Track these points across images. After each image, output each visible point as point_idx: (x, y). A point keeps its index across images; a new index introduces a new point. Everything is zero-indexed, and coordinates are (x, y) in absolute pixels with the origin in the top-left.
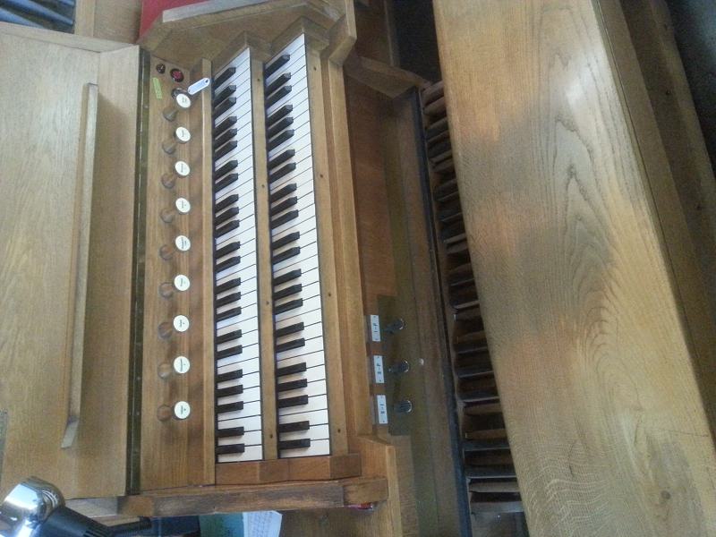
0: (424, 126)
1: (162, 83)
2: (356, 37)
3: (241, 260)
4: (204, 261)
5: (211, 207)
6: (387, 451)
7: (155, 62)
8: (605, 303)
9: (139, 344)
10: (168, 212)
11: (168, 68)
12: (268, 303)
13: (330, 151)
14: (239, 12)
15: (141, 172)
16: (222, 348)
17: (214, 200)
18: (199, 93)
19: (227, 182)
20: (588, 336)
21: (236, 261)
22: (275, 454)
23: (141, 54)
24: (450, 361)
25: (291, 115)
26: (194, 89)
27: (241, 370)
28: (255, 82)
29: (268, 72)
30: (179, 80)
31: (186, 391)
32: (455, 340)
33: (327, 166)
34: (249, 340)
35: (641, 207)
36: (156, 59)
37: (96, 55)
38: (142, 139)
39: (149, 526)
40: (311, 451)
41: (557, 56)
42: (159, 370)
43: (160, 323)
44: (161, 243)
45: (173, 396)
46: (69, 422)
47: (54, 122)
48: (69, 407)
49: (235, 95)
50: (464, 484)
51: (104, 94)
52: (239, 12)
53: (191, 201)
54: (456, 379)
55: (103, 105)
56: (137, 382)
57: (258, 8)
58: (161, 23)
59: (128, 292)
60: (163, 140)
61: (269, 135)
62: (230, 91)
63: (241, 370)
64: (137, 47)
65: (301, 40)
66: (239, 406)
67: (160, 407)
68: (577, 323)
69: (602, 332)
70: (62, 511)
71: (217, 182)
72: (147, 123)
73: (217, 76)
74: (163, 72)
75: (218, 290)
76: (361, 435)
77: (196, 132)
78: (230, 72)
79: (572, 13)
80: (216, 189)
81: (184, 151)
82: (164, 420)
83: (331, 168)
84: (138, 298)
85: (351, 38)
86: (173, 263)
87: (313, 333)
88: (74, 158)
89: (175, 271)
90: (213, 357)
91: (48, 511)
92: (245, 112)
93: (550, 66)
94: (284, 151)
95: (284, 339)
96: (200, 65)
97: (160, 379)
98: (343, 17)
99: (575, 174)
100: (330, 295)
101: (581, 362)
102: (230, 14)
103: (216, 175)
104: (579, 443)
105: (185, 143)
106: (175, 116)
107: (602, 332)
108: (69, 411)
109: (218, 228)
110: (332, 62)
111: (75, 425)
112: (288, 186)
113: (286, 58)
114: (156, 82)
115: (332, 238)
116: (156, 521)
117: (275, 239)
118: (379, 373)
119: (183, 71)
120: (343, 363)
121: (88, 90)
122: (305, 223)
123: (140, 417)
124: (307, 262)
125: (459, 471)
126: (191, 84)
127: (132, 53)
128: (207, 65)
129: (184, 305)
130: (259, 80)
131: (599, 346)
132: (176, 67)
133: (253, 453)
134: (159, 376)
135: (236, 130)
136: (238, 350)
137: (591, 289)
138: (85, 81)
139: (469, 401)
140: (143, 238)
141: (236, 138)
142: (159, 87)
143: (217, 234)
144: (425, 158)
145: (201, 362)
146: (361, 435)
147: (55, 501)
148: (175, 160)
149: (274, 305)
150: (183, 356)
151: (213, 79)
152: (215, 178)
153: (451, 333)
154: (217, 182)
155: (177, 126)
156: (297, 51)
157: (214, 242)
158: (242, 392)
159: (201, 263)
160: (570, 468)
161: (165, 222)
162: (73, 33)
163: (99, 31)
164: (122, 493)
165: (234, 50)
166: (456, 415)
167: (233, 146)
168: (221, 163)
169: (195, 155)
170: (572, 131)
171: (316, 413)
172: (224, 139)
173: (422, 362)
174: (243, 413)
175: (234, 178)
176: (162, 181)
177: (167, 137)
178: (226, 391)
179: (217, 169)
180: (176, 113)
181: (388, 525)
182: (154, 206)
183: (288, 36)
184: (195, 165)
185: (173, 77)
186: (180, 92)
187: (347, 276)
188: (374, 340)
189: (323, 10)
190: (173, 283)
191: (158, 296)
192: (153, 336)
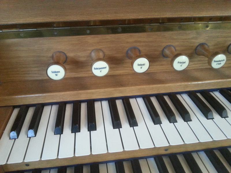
3: (158, 126)
9: (120, 30)
16: (119, 104)
17: (180, 93)
27: (137, 126)
42: (98, 50)
43: (141, 49)
56: (117, 28)
63: (137, 126)
71: (199, 95)
81: (200, 62)
89: (152, 59)
97: (89, 52)
103: (206, 93)
117: (195, 156)
129: (158, 68)
149: (165, 155)
150: (109, 71)
154: (199, 95)
158: (185, 121)
168: (186, 101)
169: (197, 74)
179: (211, 93)
191: (164, 45)
192: (128, 42)
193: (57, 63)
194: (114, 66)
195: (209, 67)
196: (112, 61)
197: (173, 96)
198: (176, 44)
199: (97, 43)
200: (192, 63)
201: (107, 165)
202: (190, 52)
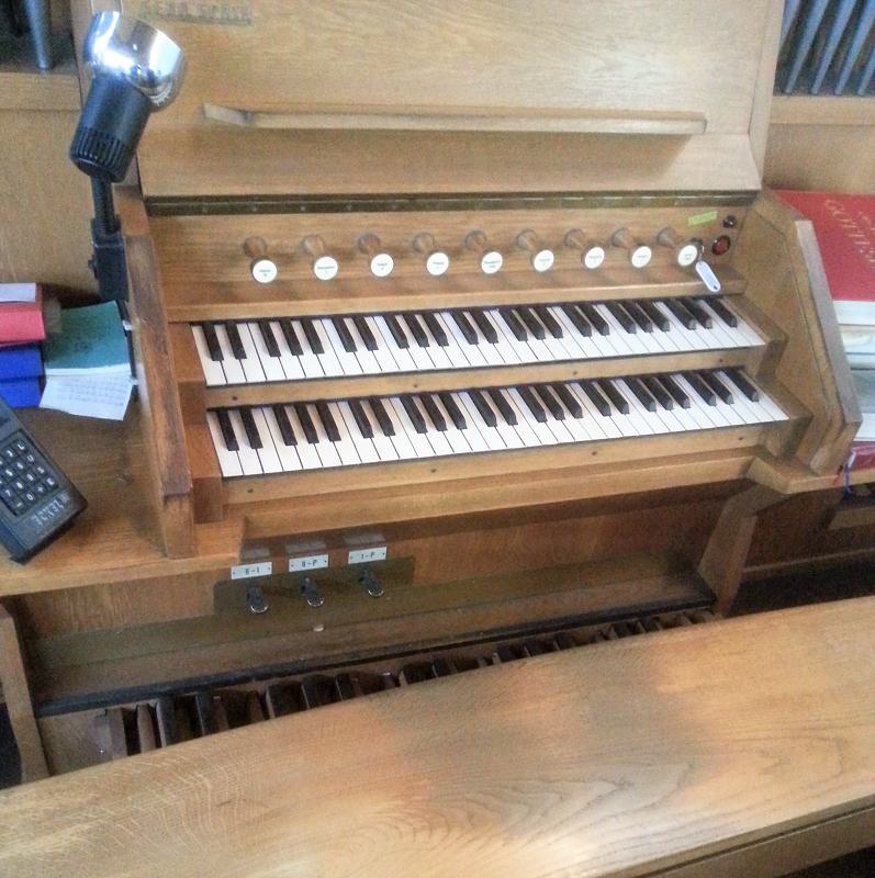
0: (661, 615)
1: (709, 226)
2: (790, 492)
4: (468, 295)
5: (543, 301)
6: (231, 555)
7: (739, 213)
8: (456, 833)
10: (532, 240)
13: (629, 464)
14: (814, 328)
15: (590, 199)
18: (699, 278)
20: (410, 814)
21: (472, 339)
22: (213, 405)
23: (747, 192)
24: (325, 668)
25: (677, 407)
26: (704, 270)
28: (717, 356)
29: (734, 373)
30: (717, 250)
31: (285, 277)
32: (357, 674)
33: (610, 460)
34: (364, 361)
35: (586, 870)
37: (746, 129)
38: (632, 199)
39: (108, 231)
40: (223, 453)
41: (768, 763)
43: (381, 237)
45: (283, 259)
46: (244, 113)
47: (650, 73)
48: (268, 113)
49: (699, 328)
50: (150, 696)
51: (692, 140)
52: (814, 328)
53: (547, 273)
54: (298, 678)
55: (674, 142)
57: (821, 353)
59: (420, 188)
60: (630, 228)
61: (646, 378)
64: (759, 187)
65: (779, 415)
66: (273, 351)
67: (263, 241)
68: (424, 800)
69: (415, 831)
70: (147, 108)
72: (652, 205)
74: (726, 225)
75: (306, 322)
76: (247, 521)
77: (644, 275)
78: (729, 319)
79: (836, 777)
82: (246, 246)
84: (411, 203)
85: (787, 485)
87: (380, 448)
88: (600, 104)
89: (454, 254)
90: (387, 310)
92: (677, 341)
93: (764, 753)
95: (371, 413)
97: (301, 239)
99: (621, 789)
100: (434, 471)
101: (372, 810)
102: (811, 316)
104: (263, 810)
105: (583, 261)
106: (664, 245)
107: (415, 831)
108: (260, 112)
109: (514, 312)
111: (238, 120)
113: (754, 396)
114: (711, 215)
115: (510, 471)
116: (116, 241)
118: (304, 564)
120: (341, 493)
121: (697, 120)
122: (529, 431)
123: (251, 212)
125: (168, 688)
126: (710, 265)
127: (752, 182)
128: (734, 286)
130: (721, 361)
131: (396, 828)
133: (213, 373)
134: (306, 237)
135: (651, 331)
136: (349, 345)
137: (471, 816)
138: (707, 116)
139: (268, 697)
140: (497, 206)
141: (640, 331)
142: (703, 221)
143: (505, 311)
144: (613, 618)
145: (331, 295)
146: (247, 521)
147: (157, 100)
148: (605, 246)
149: (414, 395)
151: (720, 296)
152: (582, 305)
153: (361, 668)
155: (652, 246)
156: (765, 411)
157: (494, 308)
158: (236, 358)
159: (464, 290)
160: (229, 802)
161: (517, 238)
162: (774, 94)
163: (779, 132)
164: (148, 191)
165: (761, 322)
166: (246, 680)
169: (611, 276)
170: (678, 784)
172: (638, 314)
173: (320, 629)
174: (265, 356)
175: (585, 331)
177: (636, 234)
178: (293, 333)
179: (549, 310)
181: (132, 561)
182: (539, 220)
183: (784, 397)
184: (549, 278)
185: (719, 240)
186: (699, 249)
187: (460, 494)
188: (351, 554)
190: (437, 251)
193: (323, 255)
194: (284, 268)
195: (580, 265)
196: (343, 256)
201: (849, 354)
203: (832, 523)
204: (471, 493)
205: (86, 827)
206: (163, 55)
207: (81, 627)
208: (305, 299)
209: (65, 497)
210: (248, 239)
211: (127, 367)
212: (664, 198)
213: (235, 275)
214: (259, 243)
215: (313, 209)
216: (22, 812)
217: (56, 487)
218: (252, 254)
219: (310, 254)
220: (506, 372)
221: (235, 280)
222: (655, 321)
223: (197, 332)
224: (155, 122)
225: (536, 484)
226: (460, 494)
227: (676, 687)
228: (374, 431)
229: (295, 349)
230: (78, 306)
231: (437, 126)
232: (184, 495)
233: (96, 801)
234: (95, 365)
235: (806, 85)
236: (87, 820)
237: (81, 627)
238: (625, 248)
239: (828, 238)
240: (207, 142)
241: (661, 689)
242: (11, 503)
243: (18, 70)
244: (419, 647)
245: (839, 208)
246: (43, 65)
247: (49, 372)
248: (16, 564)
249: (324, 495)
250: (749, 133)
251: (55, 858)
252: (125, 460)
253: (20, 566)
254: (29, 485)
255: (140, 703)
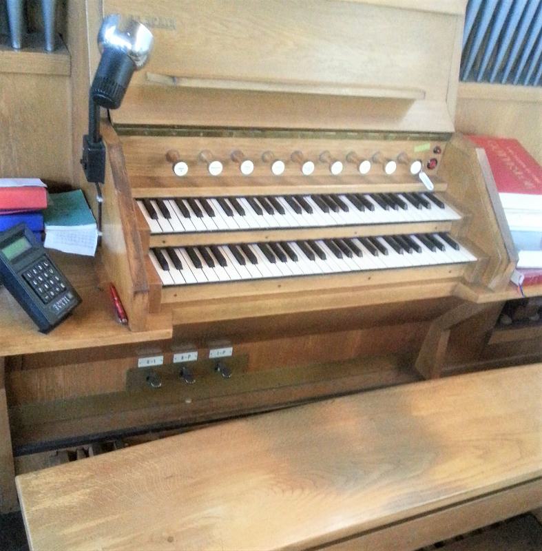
1: (426, 152)
7: (442, 145)
8: (307, 492)
11: (438, 157)
12: (267, 238)
13: (389, 285)
15: (363, 134)
18: (421, 182)
19: (225, 208)
23: (449, 133)
26: (424, 177)
36: (444, 145)
38: (385, 135)
41: (481, 452)
44: (304, 152)
48: (187, 78)
51: (415, 102)
52: (489, 207)
56: (200, 132)
58: (475, 148)
62: (426, 205)
65: (471, 258)
67: (178, 153)
70: (133, 68)
73: (436, 196)
78: (440, 204)
79: (519, 460)
80: (287, 198)
83: (375, 287)
84: (263, 132)
85: (477, 298)
86: (263, 161)
91: (134, 58)
92: (410, 217)
93: (476, 447)
94: (297, 254)
96: (441, 181)
98: (492, 291)
106: (404, 162)
108: (182, 77)
110: (456, 286)
111: (170, 82)
112: (224, 259)
114: (427, 146)
119: (436, 168)
122: (332, 263)
123: (172, 135)
124: (303, 265)
127: (449, 128)
128: (443, 187)
132: (438, 163)
133: (155, 226)
134: (202, 152)
137: (365, 471)
147: (139, 64)
148: (316, 163)
151: (433, 192)
152: (297, 197)
155: (343, 162)
159: (292, 184)
160: (171, 476)
163: (461, 101)
165: (458, 207)
167: (325, 209)
168: (244, 203)
171: (189, 273)
172: (390, 201)
175: (297, 210)
176: (325, 152)
178: (197, 206)
179: (304, 198)
180: (405, 163)
182: (332, 146)
185: (431, 160)
187: (294, 300)
188: (211, 351)
189: (497, 274)
191: (264, 150)
197: (159, 202)
198: (273, 150)
199: (461, 132)
200: (288, 170)
202: (286, 159)
203: (491, 339)
204: (300, 299)
205: (88, 490)
206: (143, 41)
207: (42, 399)
208: (201, 186)
209: (70, 296)
210: (169, 151)
211: (94, 226)
212: (402, 135)
213: (162, 172)
214: (176, 153)
215: (208, 135)
216: (46, 483)
217: (65, 289)
218: (172, 160)
219: (206, 161)
220: (318, 230)
221: (161, 175)
222: (343, 251)
223: (140, 205)
224: (136, 79)
225: (337, 295)
226: (294, 300)
227: (423, 413)
228: (246, 262)
229: (198, 214)
230: (65, 191)
231: (280, 89)
232: (145, 291)
233: (92, 477)
234: (77, 224)
235: (474, 76)
236: (88, 487)
237: (42, 399)
238: (380, 163)
239: (491, 157)
240: (152, 95)
241: (415, 413)
242: (42, 297)
243: (36, 51)
244: (252, 412)
245: (494, 145)
246: (49, 48)
247: (48, 228)
248: (41, 334)
249: (217, 299)
250: (446, 100)
251: (70, 508)
252: (97, 280)
253: (44, 335)
254: (51, 286)
255: (78, 447)
